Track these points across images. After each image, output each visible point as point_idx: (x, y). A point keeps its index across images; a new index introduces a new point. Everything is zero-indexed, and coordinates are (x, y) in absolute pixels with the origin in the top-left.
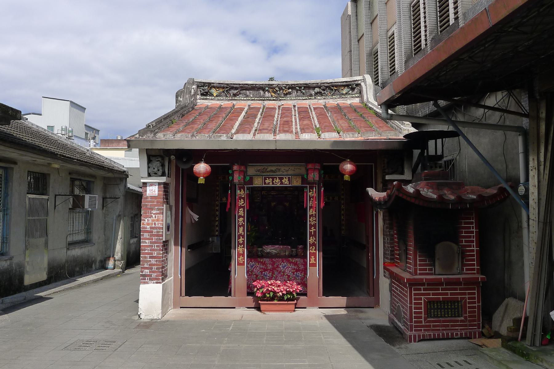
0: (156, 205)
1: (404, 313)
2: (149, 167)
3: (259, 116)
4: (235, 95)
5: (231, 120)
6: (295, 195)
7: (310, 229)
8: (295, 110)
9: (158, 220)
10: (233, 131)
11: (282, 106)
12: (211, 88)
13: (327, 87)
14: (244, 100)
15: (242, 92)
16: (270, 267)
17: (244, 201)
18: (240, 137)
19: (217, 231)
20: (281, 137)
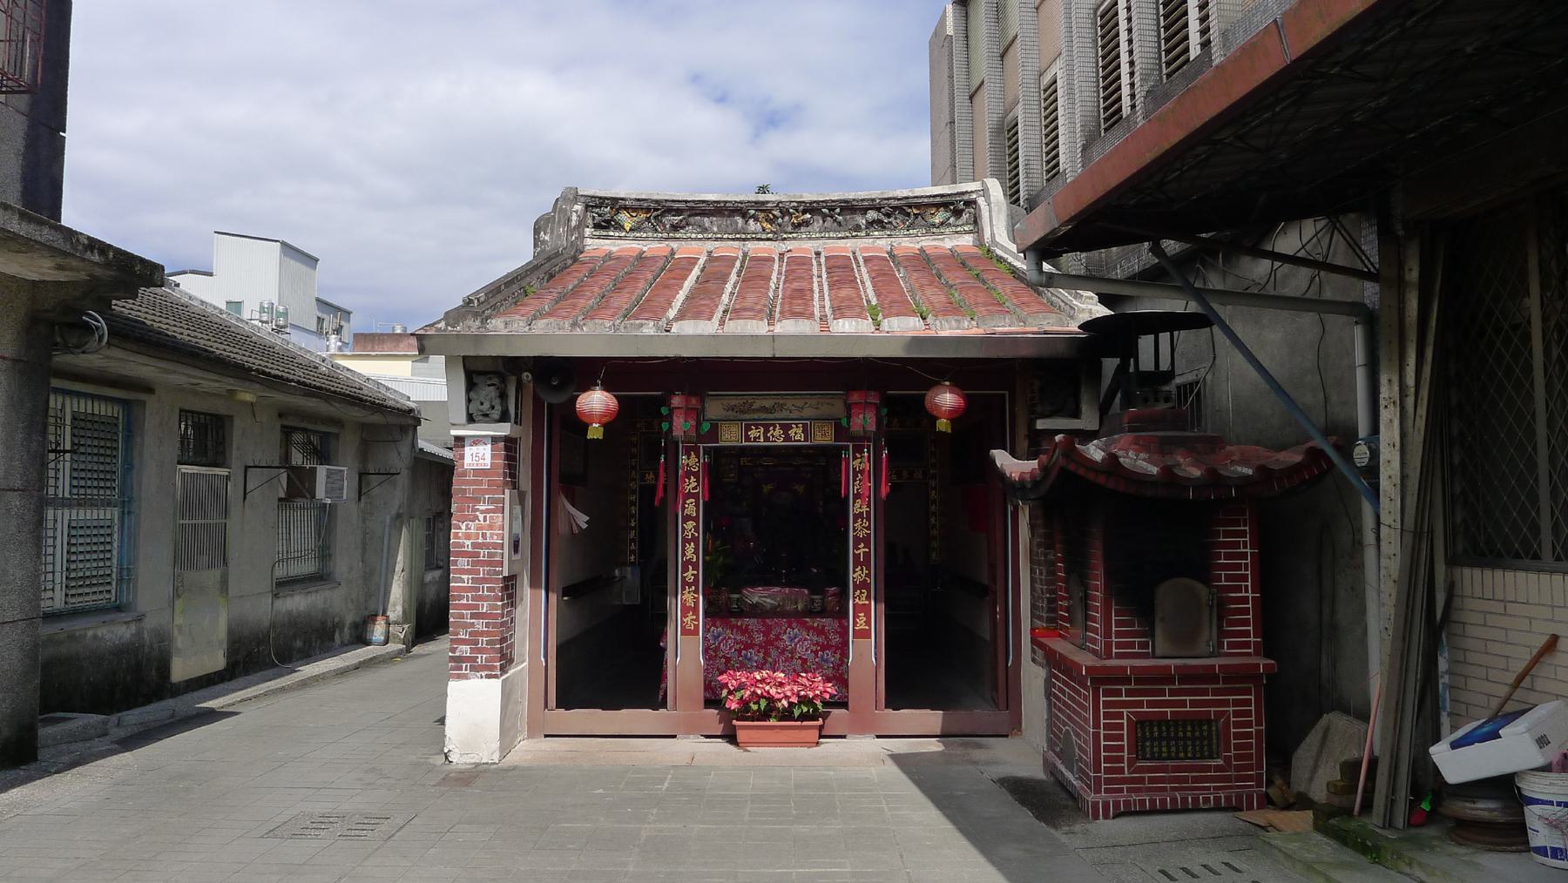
1: (1080, 747)
2: (469, 401)
3: (733, 277)
4: (675, 228)
5: (667, 287)
6: (820, 468)
7: (856, 547)
8: (819, 264)
9: (491, 527)
10: (672, 313)
13: (895, 208)
15: (692, 220)
18: (688, 328)
19: (633, 552)
20: (787, 327)
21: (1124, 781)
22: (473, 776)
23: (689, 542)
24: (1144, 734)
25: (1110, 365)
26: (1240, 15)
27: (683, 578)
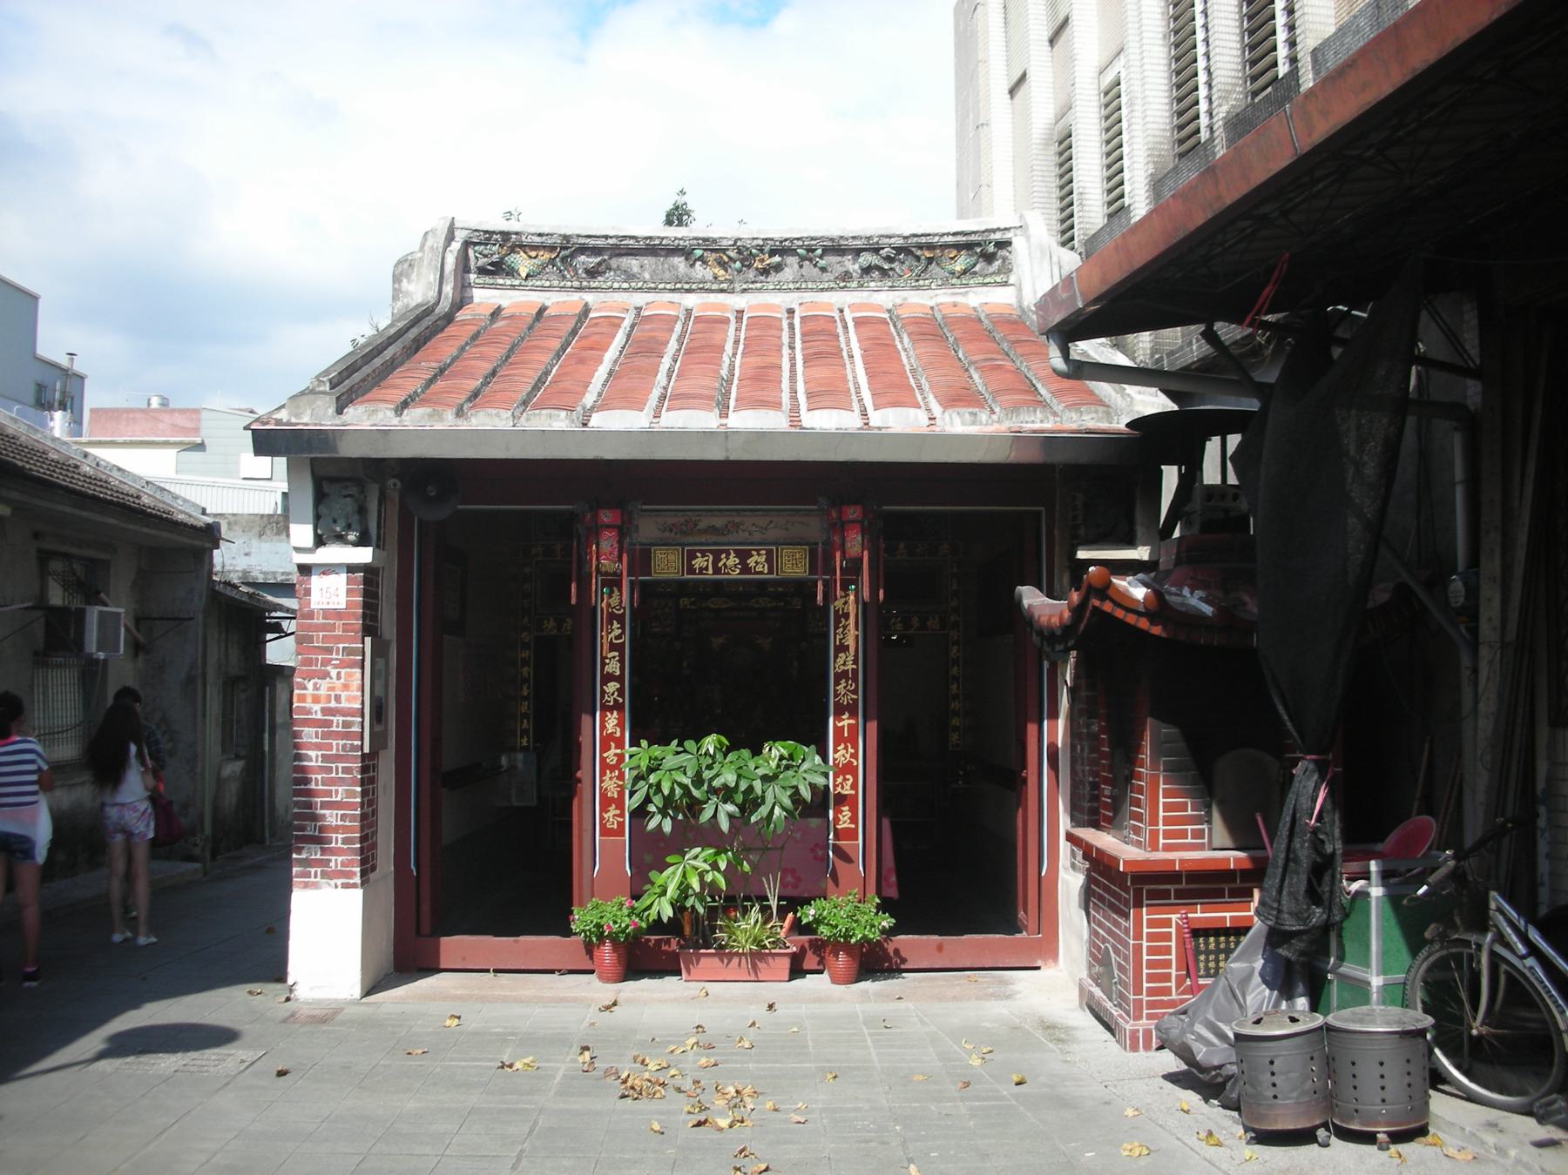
0: (339, 639)
3: (673, 345)
4: (592, 273)
5: (582, 361)
6: (794, 616)
8: (791, 327)
9: (346, 687)
10: (589, 399)
12: (512, 250)
13: (899, 250)
15: (614, 262)
17: (623, 628)
19: (525, 732)
20: (744, 420)
21: (1172, 1004)
23: (611, 709)
24: (1197, 946)
25: (1170, 477)
27: (603, 760)
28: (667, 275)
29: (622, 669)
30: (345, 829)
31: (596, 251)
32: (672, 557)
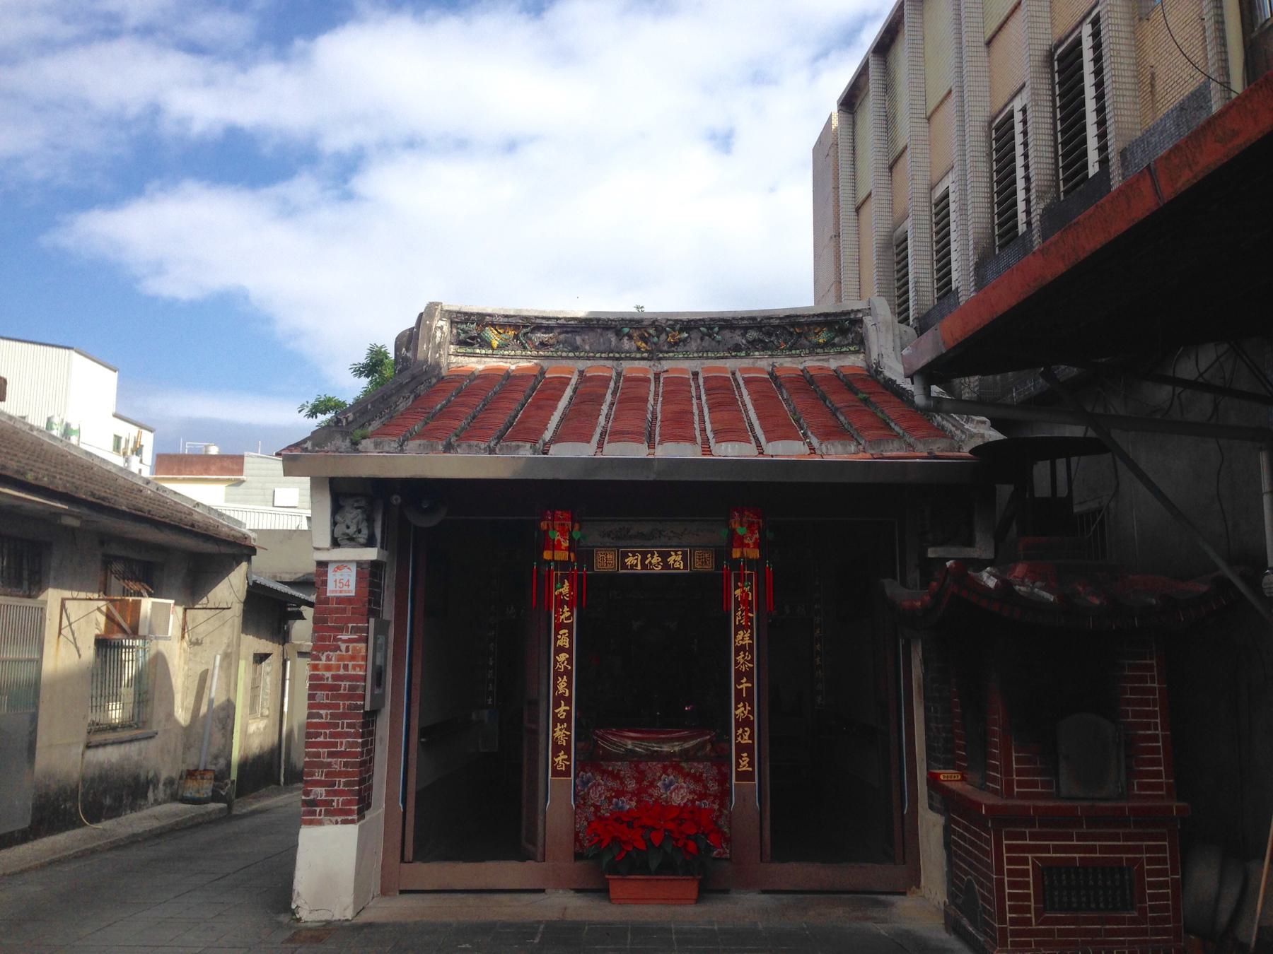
0: (349, 620)
1: (984, 898)
2: (334, 524)
3: (609, 398)
5: (540, 408)
6: (699, 600)
8: (698, 387)
9: (353, 658)
10: (548, 435)
11: (666, 375)
14: (567, 358)
16: (632, 785)
18: (562, 451)
20: (668, 451)
22: (328, 930)
25: (1005, 491)
26: (1139, 134)
28: (602, 348)
29: (571, 643)
30: (346, 774)
31: (548, 329)
32: (610, 557)
